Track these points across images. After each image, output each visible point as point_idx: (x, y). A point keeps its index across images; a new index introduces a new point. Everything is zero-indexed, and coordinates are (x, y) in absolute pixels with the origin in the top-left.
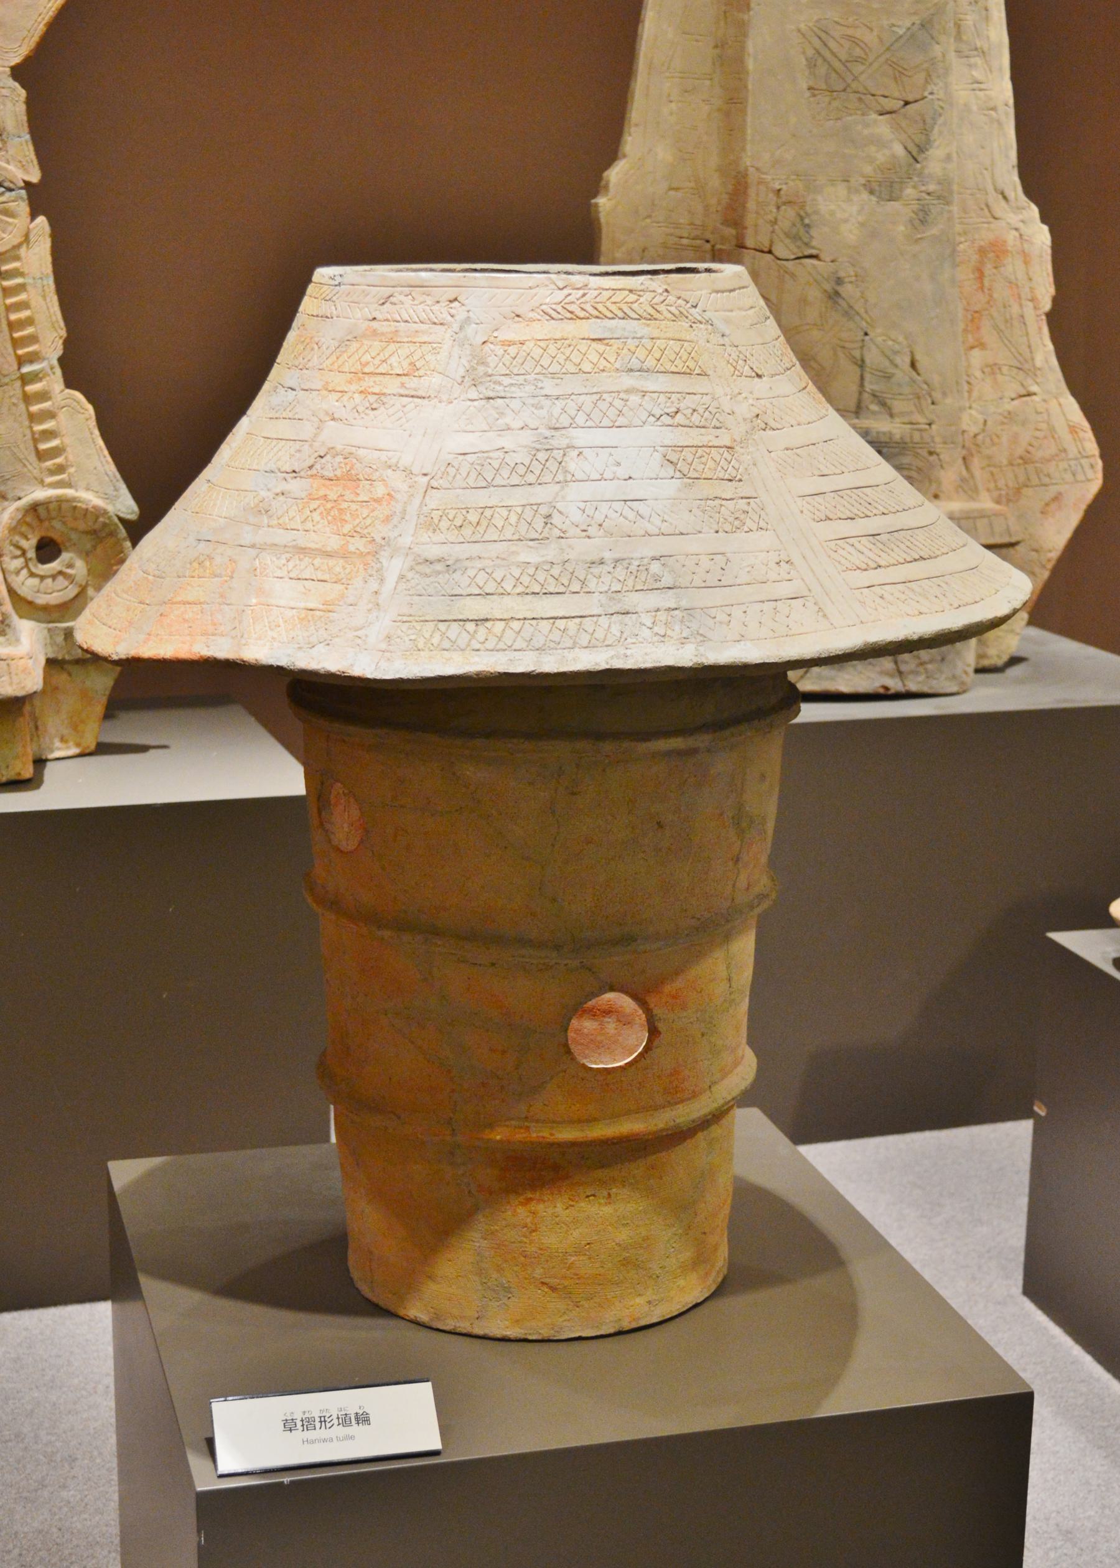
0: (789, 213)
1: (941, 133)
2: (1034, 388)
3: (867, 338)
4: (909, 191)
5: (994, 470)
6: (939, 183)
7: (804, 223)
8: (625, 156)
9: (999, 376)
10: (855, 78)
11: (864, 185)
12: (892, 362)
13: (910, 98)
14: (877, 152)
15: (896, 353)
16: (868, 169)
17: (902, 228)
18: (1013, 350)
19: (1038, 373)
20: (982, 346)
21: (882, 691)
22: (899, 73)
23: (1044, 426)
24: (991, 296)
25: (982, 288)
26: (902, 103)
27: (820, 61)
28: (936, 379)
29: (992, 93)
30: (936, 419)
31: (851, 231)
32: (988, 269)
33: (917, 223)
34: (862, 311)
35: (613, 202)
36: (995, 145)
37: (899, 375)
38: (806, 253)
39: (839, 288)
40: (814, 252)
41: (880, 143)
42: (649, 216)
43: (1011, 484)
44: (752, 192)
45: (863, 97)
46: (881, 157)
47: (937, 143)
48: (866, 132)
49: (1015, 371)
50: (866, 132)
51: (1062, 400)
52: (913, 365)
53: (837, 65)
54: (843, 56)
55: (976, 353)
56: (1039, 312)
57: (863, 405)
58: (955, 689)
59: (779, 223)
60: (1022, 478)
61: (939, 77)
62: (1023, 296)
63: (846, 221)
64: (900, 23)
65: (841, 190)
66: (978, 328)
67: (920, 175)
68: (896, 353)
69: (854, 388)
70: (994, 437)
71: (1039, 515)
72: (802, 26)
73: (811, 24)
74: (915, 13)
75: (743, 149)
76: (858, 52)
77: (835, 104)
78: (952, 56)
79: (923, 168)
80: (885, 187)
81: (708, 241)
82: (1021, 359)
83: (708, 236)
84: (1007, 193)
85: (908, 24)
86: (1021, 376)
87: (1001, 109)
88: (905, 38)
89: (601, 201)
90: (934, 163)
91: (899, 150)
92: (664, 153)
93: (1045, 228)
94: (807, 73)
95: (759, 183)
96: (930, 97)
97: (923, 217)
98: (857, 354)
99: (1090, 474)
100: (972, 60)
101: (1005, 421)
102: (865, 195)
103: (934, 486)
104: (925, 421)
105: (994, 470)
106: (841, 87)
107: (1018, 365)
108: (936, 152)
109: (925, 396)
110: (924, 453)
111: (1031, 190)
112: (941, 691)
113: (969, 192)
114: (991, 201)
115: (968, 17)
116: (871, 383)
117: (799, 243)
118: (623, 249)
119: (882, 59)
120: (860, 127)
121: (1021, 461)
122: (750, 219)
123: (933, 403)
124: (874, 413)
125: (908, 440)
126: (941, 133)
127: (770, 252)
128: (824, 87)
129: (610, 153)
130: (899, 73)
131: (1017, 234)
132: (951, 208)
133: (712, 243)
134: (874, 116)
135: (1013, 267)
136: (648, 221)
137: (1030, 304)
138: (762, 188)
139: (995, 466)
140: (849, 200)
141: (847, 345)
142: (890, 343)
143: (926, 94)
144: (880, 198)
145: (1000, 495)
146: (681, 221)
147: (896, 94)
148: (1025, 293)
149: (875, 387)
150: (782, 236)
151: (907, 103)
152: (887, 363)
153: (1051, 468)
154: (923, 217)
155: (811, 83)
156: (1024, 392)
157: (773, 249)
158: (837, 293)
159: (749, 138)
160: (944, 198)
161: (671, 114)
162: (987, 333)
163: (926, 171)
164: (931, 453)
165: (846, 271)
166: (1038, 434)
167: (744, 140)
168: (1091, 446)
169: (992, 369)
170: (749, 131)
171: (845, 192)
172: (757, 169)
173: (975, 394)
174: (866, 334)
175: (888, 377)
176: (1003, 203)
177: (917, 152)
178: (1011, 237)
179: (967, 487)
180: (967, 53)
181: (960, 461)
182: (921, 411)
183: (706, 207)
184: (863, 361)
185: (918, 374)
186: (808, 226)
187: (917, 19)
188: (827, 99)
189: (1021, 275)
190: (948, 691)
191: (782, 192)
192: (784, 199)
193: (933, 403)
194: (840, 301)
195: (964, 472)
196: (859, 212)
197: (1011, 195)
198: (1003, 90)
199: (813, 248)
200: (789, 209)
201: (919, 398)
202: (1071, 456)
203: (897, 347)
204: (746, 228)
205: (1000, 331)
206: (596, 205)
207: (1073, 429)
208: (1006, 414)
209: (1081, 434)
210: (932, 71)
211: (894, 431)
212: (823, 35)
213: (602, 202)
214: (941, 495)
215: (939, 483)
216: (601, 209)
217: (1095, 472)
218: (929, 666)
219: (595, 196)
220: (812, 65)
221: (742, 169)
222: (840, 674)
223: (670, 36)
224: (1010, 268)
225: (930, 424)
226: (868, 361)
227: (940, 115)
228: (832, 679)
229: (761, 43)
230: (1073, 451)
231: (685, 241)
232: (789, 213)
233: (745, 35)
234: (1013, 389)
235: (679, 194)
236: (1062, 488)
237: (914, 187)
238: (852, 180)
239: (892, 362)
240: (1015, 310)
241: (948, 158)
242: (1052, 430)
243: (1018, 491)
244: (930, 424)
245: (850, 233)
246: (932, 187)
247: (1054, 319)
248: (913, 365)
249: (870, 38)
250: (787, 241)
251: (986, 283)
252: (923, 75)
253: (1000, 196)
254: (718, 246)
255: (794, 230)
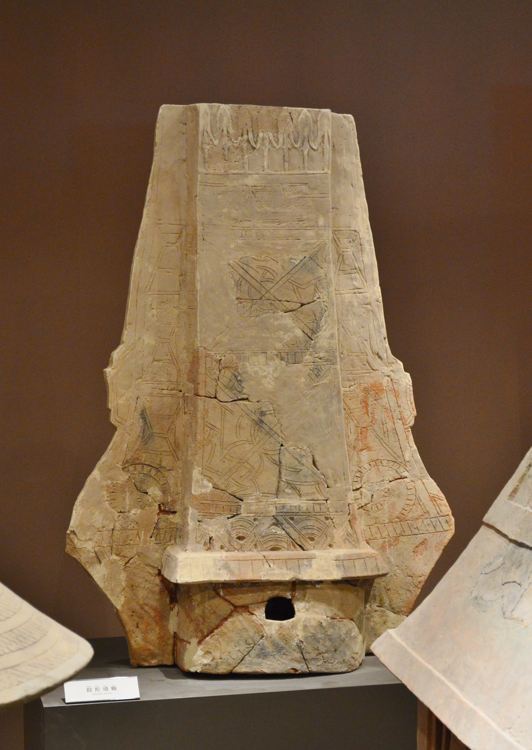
0: (228, 374)
1: (326, 322)
2: (405, 474)
3: (282, 447)
4: (307, 357)
5: (379, 526)
6: (327, 352)
7: (238, 379)
8: (123, 343)
9: (381, 467)
10: (268, 291)
11: (277, 355)
12: (299, 462)
13: (304, 302)
14: (284, 334)
15: (302, 456)
16: (279, 345)
17: (303, 380)
18: (390, 450)
19: (408, 464)
20: (369, 449)
21: (292, 672)
22: (297, 287)
23: (413, 497)
24: (373, 417)
25: (367, 412)
26: (300, 305)
27: (243, 282)
28: (330, 472)
29: (368, 295)
30: (330, 497)
31: (269, 383)
32: (371, 401)
33: (313, 376)
34: (279, 432)
35: (116, 370)
36: (371, 326)
37: (305, 470)
38: (239, 398)
39: (262, 418)
40: (245, 396)
41: (286, 329)
42: (141, 378)
43: (391, 535)
44: (202, 362)
45: (273, 302)
46: (287, 338)
47: (324, 328)
48: (276, 323)
49: (392, 463)
50: (276, 323)
51: (424, 481)
52: (314, 463)
53: (254, 283)
54: (259, 278)
55: (364, 453)
56: (406, 427)
57: (281, 489)
58: (344, 669)
59: (220, 380)
60: (398, 531)
61: (323, 288)
62: (395, 417)
63: (265, 377)
64: (296, 257)
65: (262, 358)
66: (366, 438)
67: (314, 347)
68: (302, 456)
69: (275, 479)
70: (379, 505)
71: (412, 554)
72: (231, 262)
73: (237, 261)
74: (305, 251)
75: (196, 336)
76: (269, 275)
77: (254, 307)
78: (332, 275)
79: (315, 343)
80: (292, 355)
81: (181, 391)
82: (395, 456)
83: (180, 388)
84: (380, 354)
85: (301, 257)
86: (396, 466)
87: (374, 304)
88: (300, 265)
89: (108, 370)
90: (324, 338)
91: (299, 333)
92: (149, 340)
93: (408, 374)
94: (235, 290)
95: (206, 357)
96: (318, 300)
97: (317, 373)
98: (276, 458)
99: (446, 527)
100: (353, 275)
101: (386, 495)
102: (277, 361)
103: (329, 539)
104: (323, 498)
105: (379, 526)
106: (258, 297)
107: (393, 459)
108: (324, 334)
109: (323, 482)
110: (323, 518)
111: (397, 351)
112: (335, 671)
113: (355, 354)
114: (370, 359)
115: (349, 250)
116: (286, 475)
117: (234, 392)
118: (124, 398)
119: (285, 279)
120: (272, 320)
121: (398, 520)
122: (201, 378)
123: (328, 487)
124: (288, 494)
125: (312, 510)
126: (326, 322)
127: (216, 398)
128: (247, 297)
129: (116, 342)
130: (297, 287)
131: (389, 379)
132: (335, 367)
133: (183, 392)
134: (281, 313)
135: (388, 399)
136: (140, 380)
137: (400, 422)
138: (209, 359)
139: (379, 523)
140: (267, 364)
141: (269, 453)
142: (299, 450)
143: (315, 299)
144: (288, 362)
145: (385, 542)
146: (163, 379)
147: (295, 300)
148: (396, 414)
149: (289, 478)
150: (223, 388)
151: (302, 305)
152: (296, 463)
153: (419, 523)
154: (317, 373)
155: (238, 296)
156: (398, 476)
157: (217, 396)
158: (262, 421)
159: (199, 330)
160: (331, 361)
161: (153, 316)
162: (372, 440)
163: (318, 345)
164: (327, 519)
165: (267, 407)
166: (408, 502)
167: (196, 330)
168: (446, 509)
169: (376, 463)
170: (199, 326)
171: (264, 359)
172: (205, 348)
173: (365, 478)
174: (282, 445)
175: (298, 472)
176: (379, 360)
177: (311, 334)
178: (385, 381)
179: (351, 539)
180: (350, 271)
181: (347, 522)
182: (320, 492)
183: (179, 371)
184: (280, 462)
185: (318, 469)
186: (240, 381)
187: (307, 255)
188: (249, 305)
189: (393, 404)
190: (340, 670)
191: (222, 361)
192: (223, 366)
193: (328, 487)
194: (264, 426)
195: (350, 529)
196: (274, 371)
197: (384, 356)
198: (375, 292)
199: (244, 394)
200: (227, 372)
201: (318, 484)
202: (432, 516)
203: (303, 453)
204: (199, 384)
205: (380, 439)
206: (105, 371)
207: (433, 499)
208: (386, 490)
209: (439, 502)
210: (319, 284)
211: (302, 505)
212: (245, 267)
213: (109, 371)
214: (334, 545)
215: (333, 538)
216: (107, 375)
217: (450, 526)
218: (326, 655)
219: (106, 366)
220: (238, 285)
221: (196, 347)
222: (265, 661)
223: (150, 270)
224: (385, 400)
225: (326, 500)
226: (283, 462)
227: (325, 311)
228: (260, 664)
229: (204, 272)
230: (433, 513)
231: (165, 392)
232: (228, 374)
233: (195, 268)
234: (391, 474)
235: (161, 364)
236: (426, 536)
237: (310, 355)
238: (269, 352)
239: (299, 462)
240: (390, 425)
241: (332, 336)
242: (419, 499)
243: (397, 538)
244: (326, 500)
245: (269, 384)
246: (322, 355)
247: (419, 431)
248: (314, 463)
249: (277, 267)
250: (227, 390)
251: (370, 409)
252: (312, 288)
253: (376, 356)
254: (186, 394)
255: (231, 384)
